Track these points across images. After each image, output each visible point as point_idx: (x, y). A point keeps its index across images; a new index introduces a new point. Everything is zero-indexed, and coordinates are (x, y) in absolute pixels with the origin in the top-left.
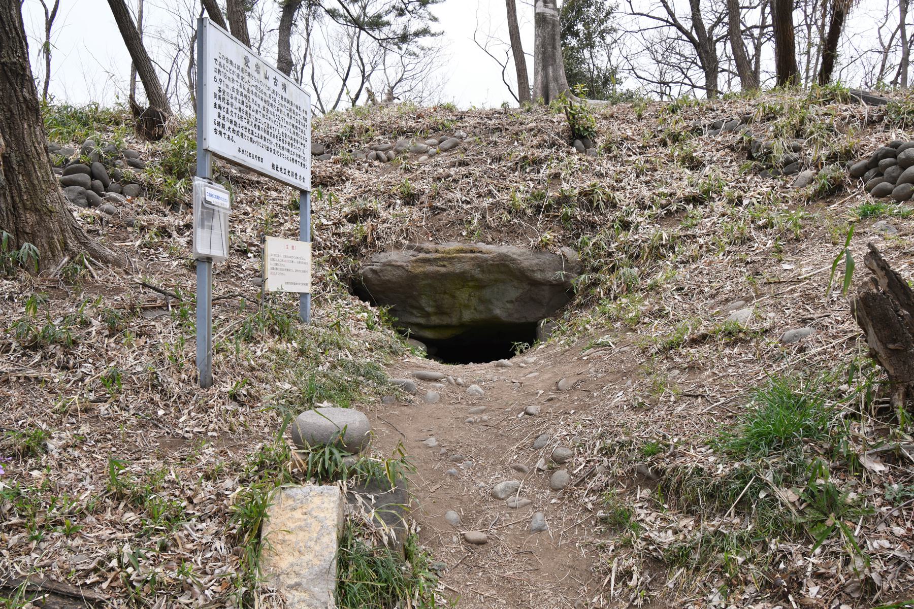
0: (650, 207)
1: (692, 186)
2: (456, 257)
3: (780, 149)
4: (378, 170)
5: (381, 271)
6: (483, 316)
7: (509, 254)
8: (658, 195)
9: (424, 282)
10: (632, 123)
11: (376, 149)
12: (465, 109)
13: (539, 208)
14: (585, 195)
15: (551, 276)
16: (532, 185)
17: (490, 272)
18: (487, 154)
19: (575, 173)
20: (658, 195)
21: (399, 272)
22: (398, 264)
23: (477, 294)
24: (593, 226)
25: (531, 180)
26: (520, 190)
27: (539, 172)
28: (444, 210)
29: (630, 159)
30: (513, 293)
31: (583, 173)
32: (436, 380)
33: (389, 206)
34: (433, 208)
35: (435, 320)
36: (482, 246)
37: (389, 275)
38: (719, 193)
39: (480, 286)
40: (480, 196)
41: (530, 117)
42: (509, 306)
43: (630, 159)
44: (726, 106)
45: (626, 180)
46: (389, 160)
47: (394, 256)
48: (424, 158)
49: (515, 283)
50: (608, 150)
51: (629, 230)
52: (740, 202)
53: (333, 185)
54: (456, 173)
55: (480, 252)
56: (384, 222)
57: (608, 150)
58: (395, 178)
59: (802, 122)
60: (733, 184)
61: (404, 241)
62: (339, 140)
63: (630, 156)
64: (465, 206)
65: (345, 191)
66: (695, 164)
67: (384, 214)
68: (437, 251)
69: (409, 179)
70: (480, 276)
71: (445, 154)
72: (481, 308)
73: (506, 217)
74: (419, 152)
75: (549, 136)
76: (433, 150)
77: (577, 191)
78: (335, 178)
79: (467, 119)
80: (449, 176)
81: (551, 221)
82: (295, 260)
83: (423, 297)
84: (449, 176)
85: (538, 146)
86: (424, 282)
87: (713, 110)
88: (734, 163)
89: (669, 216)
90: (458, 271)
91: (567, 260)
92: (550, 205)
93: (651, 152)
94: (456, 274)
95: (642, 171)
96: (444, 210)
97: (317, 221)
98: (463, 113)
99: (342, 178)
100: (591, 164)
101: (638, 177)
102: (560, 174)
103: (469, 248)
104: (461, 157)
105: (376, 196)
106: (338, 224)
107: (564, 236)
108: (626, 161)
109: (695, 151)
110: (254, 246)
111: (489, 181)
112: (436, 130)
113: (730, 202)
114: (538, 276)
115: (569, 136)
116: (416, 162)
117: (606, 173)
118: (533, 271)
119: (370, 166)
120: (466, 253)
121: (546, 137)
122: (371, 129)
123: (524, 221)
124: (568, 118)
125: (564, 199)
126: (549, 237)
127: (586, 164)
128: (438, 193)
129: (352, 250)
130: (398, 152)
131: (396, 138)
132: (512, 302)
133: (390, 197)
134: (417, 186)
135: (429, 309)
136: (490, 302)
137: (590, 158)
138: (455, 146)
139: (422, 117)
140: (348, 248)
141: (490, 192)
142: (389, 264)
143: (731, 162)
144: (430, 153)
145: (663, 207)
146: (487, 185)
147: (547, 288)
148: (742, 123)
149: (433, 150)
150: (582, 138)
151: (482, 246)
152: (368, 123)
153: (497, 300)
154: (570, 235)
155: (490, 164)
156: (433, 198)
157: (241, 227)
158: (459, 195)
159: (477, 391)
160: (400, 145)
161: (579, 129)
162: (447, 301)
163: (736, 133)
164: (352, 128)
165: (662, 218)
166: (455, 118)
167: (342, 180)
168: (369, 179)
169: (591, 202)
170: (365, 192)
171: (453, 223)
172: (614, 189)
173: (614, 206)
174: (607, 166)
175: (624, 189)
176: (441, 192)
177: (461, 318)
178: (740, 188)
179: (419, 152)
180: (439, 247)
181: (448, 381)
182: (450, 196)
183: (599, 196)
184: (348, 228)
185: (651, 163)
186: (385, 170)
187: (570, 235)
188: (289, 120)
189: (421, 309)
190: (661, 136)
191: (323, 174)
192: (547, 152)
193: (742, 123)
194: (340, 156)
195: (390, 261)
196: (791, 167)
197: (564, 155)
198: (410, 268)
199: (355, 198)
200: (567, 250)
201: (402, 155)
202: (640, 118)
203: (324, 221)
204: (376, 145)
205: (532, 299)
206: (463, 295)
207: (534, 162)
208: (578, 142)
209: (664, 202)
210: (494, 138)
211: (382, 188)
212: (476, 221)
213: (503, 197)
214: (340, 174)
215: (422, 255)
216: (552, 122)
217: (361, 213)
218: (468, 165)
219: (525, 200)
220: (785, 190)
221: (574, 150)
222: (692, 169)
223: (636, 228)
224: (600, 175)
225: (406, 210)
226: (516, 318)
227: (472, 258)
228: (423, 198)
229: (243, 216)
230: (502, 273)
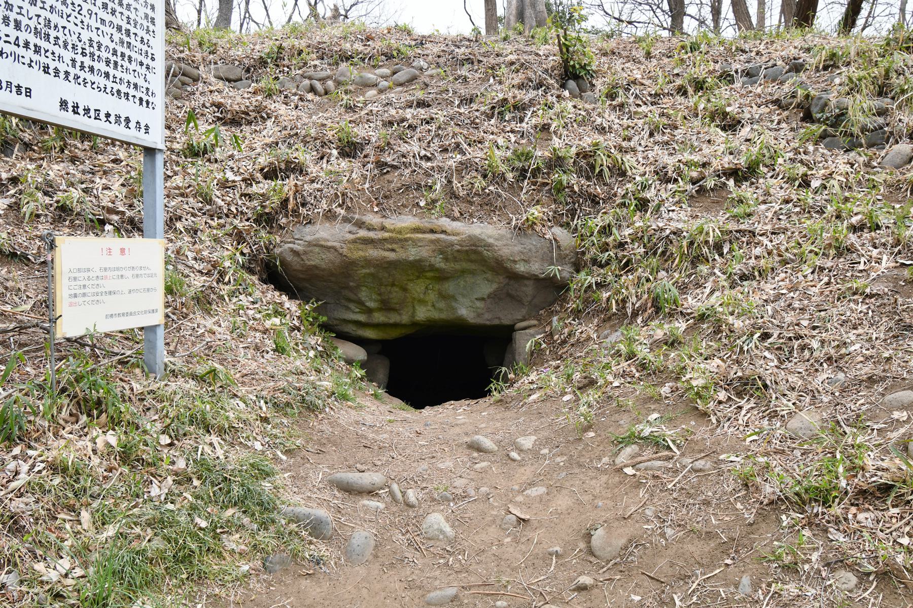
0: (676, 180)
1: (731, 153)
2: (410, 239)
3: (861, 109)
4: (311, 106)
5: (305, 253)
6: (443, 316)
7: (483, 237)
8: (686, 164)
9: (364, 271)
10: (640, 62)
11: (310, 78)
12: (426, 34)
13: (523, 171)
14: (585, 157)
15: (535, 268)
16: (513, 139)
17: (455, 259)
18: (455, 93)
19: (571, 128)
20: (686, 164)
21: (330, 256)
22: (330, 244)
23: (437, 287)
24: (594, 200)
25: (512, 131)
26: (498, 147)
27: (522, 121)
28: (395, 168)
29: (640, 110)
30: (486, 288)
31: (579, 125)
32: (371, 492)
33: (322, 158)
34: (380, 165)
35: (379, 317)
36: (445, 222)
37: (317, 259)
38: (771, 167)
39: (441, 277)
40: (445, 150)
41: (509, 48)
42: (479, 304)
43: (640, 110)
44: (762, 47)
45: (636, 138)
46: (326, 93)
47: (324, 232)
48: (372, 92)
49: (489, 275)
50: (611, 96)
51: (646, 211)
52: (805, 183)
53: (250, 123)
54: (413, 117)
55: (444, 232)
56: (313, 181)
57: (611, 96)
58: (332, 121)
59: (887, 76)
60: (791, 155)
61: (339, 210)
62: (263, 62)
63: (639, 105)
64: (426, 165)
65: (264, 133)
66: (731, 125)
67: (313, 170)
68: (383, 228)
69: (350, 122)
70: (443, 265)
71: (400, 89)
72: (442, 305)
73: (479, 183)
74: (367, 85)
75: (535, 73)
76: (384, 84)
77: (574, 150)
78: (253, 114)
79: (428, 45)
80: (403, 120)
81: (539, 191)
82: (129, 273)
83: (364, 289)
84: (403, 120)
85: (521, 87)
86: (364, 271)
87: (744, 51)
88: (784, 125)
89: (702, 194)
90: (411, 258)
91: (559, 247)
92: (538, 169)
93: (666, 101)
94: (410, 262)
95: (657, 128)
96: (395, 168)
97: (220, 176)
98: (424, 37)
99: (262, 115)
100: (589, 114)
101: (651, 135)
102: (549, 125)
103: (428, 226)
104: (420, 95)
105: (305, 143)
106: (249, 181)
107: (555, 212)
108: (636, 113)
109: (729, 105)
110: (117, 213)
111: (457, 130)
112: (389, 57)
113: (791, 180)
114: (521, 268)
115: (561, 75)
116: (361, 98)
117: (610, 128)
118: (515, 262)
119: (301, 99)
120: (424, 232)
121: (531, 74)
122: (306, 50)
123: (504, 189)
124: (561, 50)
125: (556, 162)
126: (536, 214)
127: (584, 113)
128: (389, 144)
129: (266, 220)
130: (338, 83)
131: (337, 64)
132: (483, 299)
133: (323, 144)
134: (360, 132)
135: (371, 304)
136: (453, 298)
137: (587, 106)
138: (412, 79)
139: (372, 39)
140: (261, 216)
141: (458, 145)
142: (316, 244)
143: (779, 123)
144: (380, 86)
145: (694, 182)
146: (455, 135)
147: (530, 283)
148: (789, 71)
149: (384, 84)
150: (576, 77)
151: (445, 222)
152: (302, 44)
153: (464, 296)
154: (562, 210)
155: (459, 106)
156: (381, 149)
157: (104, 181)
158: (416, 149)
159: (442, 532)
160: (342, 74)
161: (574, 66)
162: (396, 295)
163: (782, 83)
164: (280, 47)
165: (692, 196)
166: (413, 43)
167: (262, 117)
168: (299, 118)
169: (593, 167)
170: (291, 136)
171: (408, 188)
172: (620, 149)
173: (623, 174)
174: (610, 117)
175: (634, 150)
176: (392, 142)
177: (413, 315)
178: (801, 162)
179: (367, 85)
180: (388, 223)
181: (391, 494)
182: (404, 148)
183: (603, 160)
184: (263, 187)
185: (668, 117)
186: (321, 107)
187: (562, 210)
188: (108, 18)
189: (360, 303)
190: (679, 82)
191: (236, 107)
192: (532, 94)
193: (789, 71)
194: (262, 84)
195: (318, 240)
196: (879, 138)
197: (555, 99)
198: (345, 251)
199: (277, 144)
200: (557, 230)
201: (343, 88)
202: (648, 56)
203: (230, 176)
204: (311, 72)
205: (509, 295)
206: (417, 288)
207: (516, 107)
208: (572, 84)
209: (695, 174)
210: (464, 71)
211: (313, 132)
212: (438, 187)
213: (475, 154)
214: (259, 109)
215: (363, 233)
216: (537, 55)
217: (283, 166)
218: (429, 106)
219: (506, 160)
220: (869, 169)
221: (566, 93)
222: (724, 129)
223: (657, 209)
224: (602, 130)
225: (344, 164)
226: (487, 319)
227: (432, 241)
228: (368, 150)
229: (110, 165)
230: (471, 261)
